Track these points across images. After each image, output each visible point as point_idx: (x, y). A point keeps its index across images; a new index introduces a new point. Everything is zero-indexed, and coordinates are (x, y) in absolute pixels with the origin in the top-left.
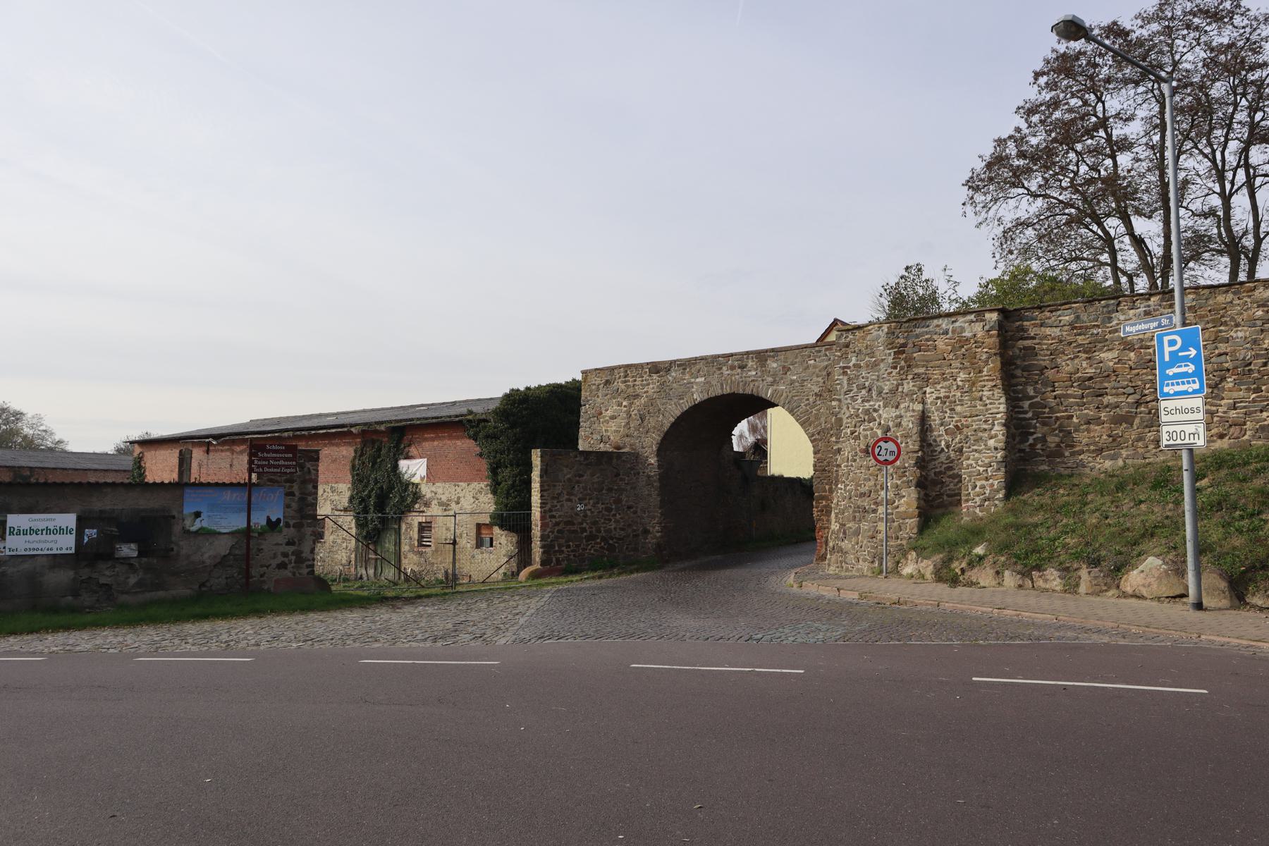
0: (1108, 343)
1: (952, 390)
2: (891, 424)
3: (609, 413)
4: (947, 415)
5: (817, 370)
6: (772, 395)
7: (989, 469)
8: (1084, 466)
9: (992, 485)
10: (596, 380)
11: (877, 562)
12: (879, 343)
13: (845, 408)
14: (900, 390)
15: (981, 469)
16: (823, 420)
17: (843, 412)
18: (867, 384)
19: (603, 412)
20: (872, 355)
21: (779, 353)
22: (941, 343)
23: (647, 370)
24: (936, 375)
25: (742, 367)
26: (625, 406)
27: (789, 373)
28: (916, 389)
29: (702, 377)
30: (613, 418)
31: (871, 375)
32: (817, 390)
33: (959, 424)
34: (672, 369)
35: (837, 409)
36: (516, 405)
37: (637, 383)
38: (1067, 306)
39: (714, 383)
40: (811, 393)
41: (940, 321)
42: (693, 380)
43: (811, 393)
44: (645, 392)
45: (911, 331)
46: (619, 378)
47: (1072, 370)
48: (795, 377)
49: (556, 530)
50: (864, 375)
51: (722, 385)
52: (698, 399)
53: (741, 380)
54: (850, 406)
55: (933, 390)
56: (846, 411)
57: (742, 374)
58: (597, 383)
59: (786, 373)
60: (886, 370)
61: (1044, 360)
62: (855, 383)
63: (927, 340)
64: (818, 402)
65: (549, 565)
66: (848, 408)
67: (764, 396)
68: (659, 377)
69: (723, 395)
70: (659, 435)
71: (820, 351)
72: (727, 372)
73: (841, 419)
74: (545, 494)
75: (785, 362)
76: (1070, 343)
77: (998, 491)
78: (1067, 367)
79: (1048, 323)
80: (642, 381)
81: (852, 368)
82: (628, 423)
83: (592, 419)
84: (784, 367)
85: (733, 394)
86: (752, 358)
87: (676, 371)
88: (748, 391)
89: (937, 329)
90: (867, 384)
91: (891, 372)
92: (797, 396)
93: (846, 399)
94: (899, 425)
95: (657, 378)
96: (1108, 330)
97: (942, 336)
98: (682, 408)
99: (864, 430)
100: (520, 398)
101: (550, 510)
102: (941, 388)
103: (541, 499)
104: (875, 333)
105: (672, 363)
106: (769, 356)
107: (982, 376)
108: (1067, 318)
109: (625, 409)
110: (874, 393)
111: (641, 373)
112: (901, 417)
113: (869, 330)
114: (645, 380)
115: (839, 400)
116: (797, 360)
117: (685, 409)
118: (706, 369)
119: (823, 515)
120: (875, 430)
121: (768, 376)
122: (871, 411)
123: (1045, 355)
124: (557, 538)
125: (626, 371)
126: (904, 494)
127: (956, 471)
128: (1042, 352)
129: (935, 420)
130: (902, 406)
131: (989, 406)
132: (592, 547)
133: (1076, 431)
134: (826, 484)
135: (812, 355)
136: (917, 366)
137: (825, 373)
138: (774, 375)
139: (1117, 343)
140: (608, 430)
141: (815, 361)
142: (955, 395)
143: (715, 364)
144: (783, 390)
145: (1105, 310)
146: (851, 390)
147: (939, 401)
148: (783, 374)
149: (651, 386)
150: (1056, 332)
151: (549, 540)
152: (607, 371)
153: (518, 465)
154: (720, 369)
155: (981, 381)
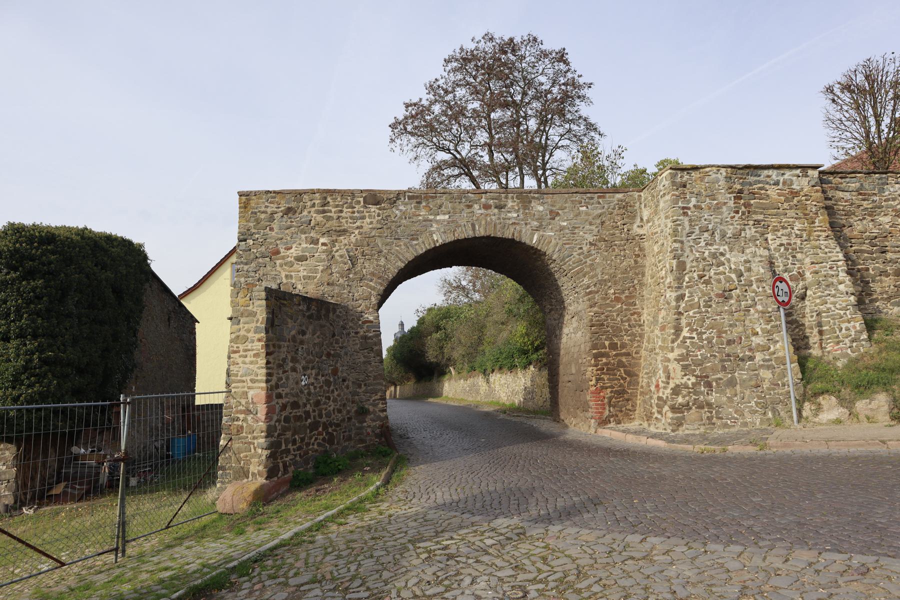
0: (884, 209)
1: (792, 238)
2: (742, 268)
3: (294, 252)
4: (790, 262)
5: (591, 217)
6: (539, 241)
7: (848, 312)
8: (880, 312)
9: (854, 327)
10: (267, 207)
11: (770, 413)
12: (719, 186)
13: (688, 250)
14: (743, 235)
15: (842, 312)
16: (599, 271)
17: (686, 255)
18: (710, 227)
19: (282, 250)
20: (712, 197)
21: (545, 196)
22: (773, 192)
23: (361, 200)
24: (774, 222)
25: (500, 207)
26: (323, 244)
27: (557, 218)
28: (758, 235)
29: (444, 214)
30: (300, 259)
31: (714, 218)
32: (591, 238)
33: (801, 271)
34: (399, 202)
35: (680, 252)
36: (36, 244)
37: (343, 215)
38: (853, 175)
39: (462, 222)
40: (585, 242)
41: (770, 172)
42: (431, 217)
43: (585, 242)
44: (357, 228)
45: (745, 178)
46: (313, 206)
47: (863, 230)
48: (565, 224)
49: (283, 417)
50: (706, 217)
51: (473, 225)
52: (440, 241)
53: (498, 221)
54: (693, 249)
55: (775, 237)
56: (690, 254)
57: (500, 214)
58: (269, 210)
59: (554, 219)
60: (729, 214)
61: (841, 219)
62: (697, 225)
63: (761, 188)
64: (593, 252)
65: (277, 475)
66: (692, 251)
67: (528, 242)
68: (379, 209)
69: (475, 238)
70: (381, 284)
71: (592, 198)
72: (480, 211)
73: (684, 263)
74: (271, 358)
75: (552, 206)
76: (859, 206)
77: (861, 332)
78: (859, 227)
79: (840, 188)
80: (353, 212)
81: (693, 209)
82: (329, 267)
83: (260, 260)
84: (551, 212)
85: (489, 237)
86: (513, 198)
87: (407, 204)
88: (508, 235)
89: (768, 180)
90: (710, 227)
91: (734, 217)
92: (568, 244)
93: (689, 241)
94: (749, 270)
95: (377, 211)
96: (884, 198)
97: (773, 187)
98: (416, 250)
99: (715, 274)
100: (41, 236)
101: (277, 386)
102: (782, 235)
103: (267, 368)
104: (714, 176)
105: (399, 194)
106: (534, 198)
107: (815, 227)
108: (853, 185)
109: (324, 248)
110: (717, 237)
111: (351, 203)
112: (750, 262)
113: (707, 172)
114: (358, 212)
115: (682, 242)
116: (567, 205)
117: (421, 252)
118: (450, 205)
119: (603, 373)
120: (727, 274)
121: (533, 220)
122: (718, 254)
123: (842, 215)
124: (285, 430)
125: (325, 198)
126: (777, 339)
127: (794, 317)
128: (839, 212)
129: (779, 267)
130: (748, 251)
131: (829, 254)
132: (316, 439)
133: (873, 281)
134: (606, 340)
135: (583, 201)
136: (755, 213)
137: (599, 221)
138: (540, 219)
139: (890, 210)
140: (291, 276)
141: (587, 208)
142: (795, 243)
143: (464, 200)
144: (551, 236)
145: (880, 181)
146: (694, 232)
147: (782, 249)
148: (551, 219)
149: (368, 220)
150: (847, 196)
151: (276, 434)
152: (288, 196)
153: (35, 336)
154: (469, 207)
155: (815, 231)
